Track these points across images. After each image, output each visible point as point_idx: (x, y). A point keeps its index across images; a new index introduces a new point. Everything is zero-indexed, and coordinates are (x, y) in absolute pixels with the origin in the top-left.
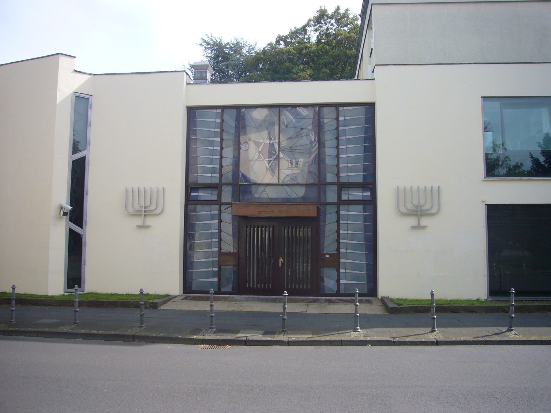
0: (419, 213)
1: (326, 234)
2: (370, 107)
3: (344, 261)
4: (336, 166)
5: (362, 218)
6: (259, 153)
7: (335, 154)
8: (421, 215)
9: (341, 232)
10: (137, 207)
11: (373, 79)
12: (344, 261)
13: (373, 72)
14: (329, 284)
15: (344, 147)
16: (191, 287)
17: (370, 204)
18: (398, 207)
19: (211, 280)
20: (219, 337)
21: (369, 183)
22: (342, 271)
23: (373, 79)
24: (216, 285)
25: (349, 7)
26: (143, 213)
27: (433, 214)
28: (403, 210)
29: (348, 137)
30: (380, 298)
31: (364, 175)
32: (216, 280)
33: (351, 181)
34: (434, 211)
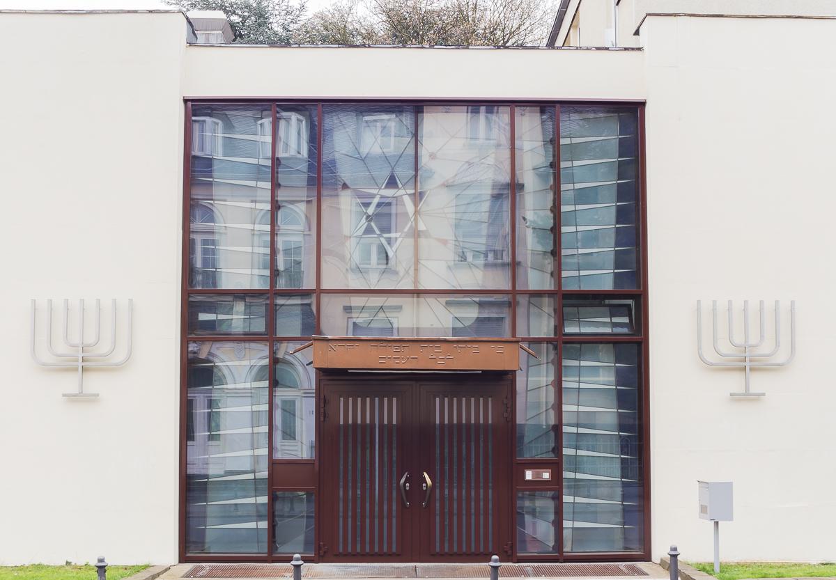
0: (747, 364)
1: (526, 440)
2: (630, 114)
3: (568, 164)
4: (552, 230)
5: (616, 444)
6: (369, 218)
7: (550, 223)
8: (751, 369)
9: (565, 408)
10: (62, 348)
11: (639, 49)
12: (568, 164)
13: (637, 33)
14: (540, 530)
15: (571, 208)
16: (201, 542)
17: (632, 351)
18: (699, 348)
19: (252, 525)
20: (342, 455)
21: (630, 296)
22: (567, 499)
23: (639, 49)
24: (265, 537)
25: (674, 544)
26: (80, 364)
27: (778, 367)
28: (711, 357)
29: (578, 186)
30: (659, 562)
31: (615, 274)
32: (264, 525)
33: (585, 287)
34: (780, 358)
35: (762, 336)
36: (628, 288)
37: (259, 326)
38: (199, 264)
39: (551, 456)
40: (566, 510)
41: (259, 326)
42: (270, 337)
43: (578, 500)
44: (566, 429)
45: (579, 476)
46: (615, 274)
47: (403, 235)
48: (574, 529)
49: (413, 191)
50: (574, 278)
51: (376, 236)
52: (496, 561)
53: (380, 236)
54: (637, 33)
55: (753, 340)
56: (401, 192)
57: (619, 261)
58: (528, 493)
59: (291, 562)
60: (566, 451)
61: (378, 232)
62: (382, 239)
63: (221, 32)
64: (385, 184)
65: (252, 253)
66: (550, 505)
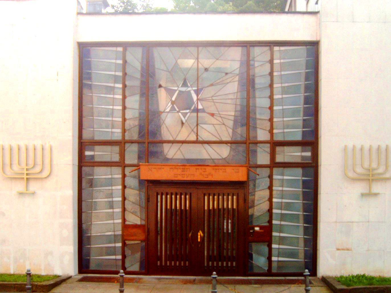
2: (314, 46)
6: (173, 103)
14: (260, 261)
16: (88, 266)
22: (274, 246)
28: (351, 174)
31: (303, 131)
35: (379, 164)
36: (310, 139)
37: (116, 158)
38: (251, 104)
39: (267, 224)
40: (274, 252)
41: (116, 158)
42: (122, 164)
43: (281, 247)
44: (275, 211)
45: (282, 235)
46: (303, 131)
47: (190, 111)
48: (278, 261)
49: (196, 88)
50: (279, 134)
51: (176, 112)
52: (215, 275)
53: (178, 112)
54: (317, 3)
55: (374, 165)
56: (189, 89)
57: (305, 124)
58: (229, 241)
59: (119, 274)
60: (274, 222)
61: (177, 110)
62: (180, 114)
63: (102, 3)
64: (181, 85)
65: (236, 104)
66: (266, 249)
